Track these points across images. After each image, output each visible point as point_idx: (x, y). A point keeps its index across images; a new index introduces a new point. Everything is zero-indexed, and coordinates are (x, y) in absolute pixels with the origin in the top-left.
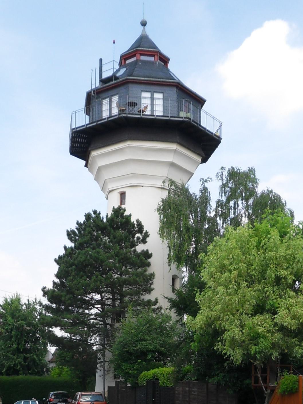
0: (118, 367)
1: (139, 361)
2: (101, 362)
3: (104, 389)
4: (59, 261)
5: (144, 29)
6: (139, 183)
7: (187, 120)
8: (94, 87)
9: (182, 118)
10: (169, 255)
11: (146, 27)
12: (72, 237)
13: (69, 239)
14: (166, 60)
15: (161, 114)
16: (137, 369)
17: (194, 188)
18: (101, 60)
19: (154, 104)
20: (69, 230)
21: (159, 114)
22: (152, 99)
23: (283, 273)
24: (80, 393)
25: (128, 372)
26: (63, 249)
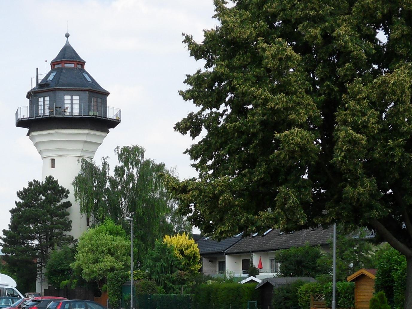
0: (49, 278)
1: (60, 275)
2: (39, 274)
3: (42, 291)
4: (13, 211)
5: (67, 39)
6: (61, 161)
7: (94, 117)
8: (33, 88)
9: (91, 115)
10: (81, 208)
11: (69, 38)
12: (20, 196)
13: (18, 196)
14: (83, 64)
15: (78, 114)
16: (59, 280)
17: (98, 164)
18: (37, 69)
19: (72, 104)
20: (18, 191)
21: (76, 114)
22: (72, 100)
23: (104, 249)
24: (28, 293)
25: (54, 282)
26: (15, 203)
